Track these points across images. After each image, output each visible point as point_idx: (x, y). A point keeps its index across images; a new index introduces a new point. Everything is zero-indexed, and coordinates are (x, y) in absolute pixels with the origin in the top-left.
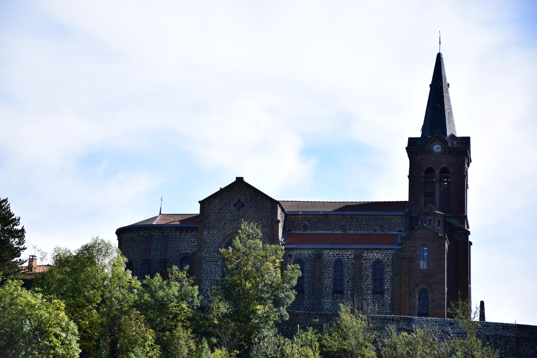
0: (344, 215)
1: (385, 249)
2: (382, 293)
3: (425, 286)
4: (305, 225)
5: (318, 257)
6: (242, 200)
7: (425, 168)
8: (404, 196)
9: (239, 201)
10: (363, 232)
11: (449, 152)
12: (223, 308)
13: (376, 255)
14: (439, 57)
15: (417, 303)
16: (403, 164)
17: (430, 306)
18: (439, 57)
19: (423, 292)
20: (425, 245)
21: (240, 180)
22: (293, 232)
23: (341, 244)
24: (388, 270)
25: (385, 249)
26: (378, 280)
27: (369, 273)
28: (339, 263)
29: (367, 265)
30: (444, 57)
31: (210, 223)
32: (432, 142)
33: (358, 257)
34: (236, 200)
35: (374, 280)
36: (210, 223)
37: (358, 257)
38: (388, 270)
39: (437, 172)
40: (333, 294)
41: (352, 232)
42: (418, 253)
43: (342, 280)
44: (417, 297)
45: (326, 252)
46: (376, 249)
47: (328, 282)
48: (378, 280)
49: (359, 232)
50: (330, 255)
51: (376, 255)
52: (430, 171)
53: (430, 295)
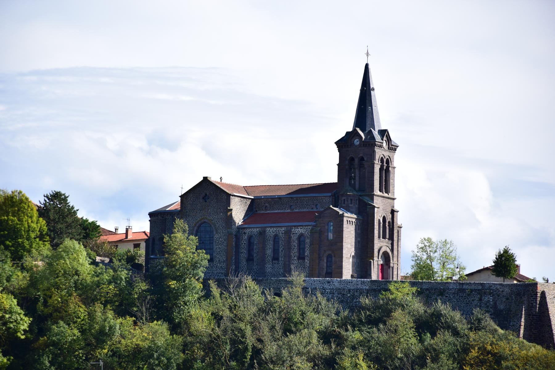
0: (292, 198)
1: (306, 226)
2: (303, 259)
3: (330, 252)
4: (266, 207)
5: (262, 233)
6: (208, 194)
7: (348, 158)
8: (334, 179)
9: (206, 194)
10: (305, 210)
11: (364, 145)
12: (143, 286)
13: (300, 230)
14: (367, 66)
15: (325, 265)
16: (334, 156)
17: (333, 267)
18: (367, 66)
19: (329, 256)
20: (330, 221)
21: (205, 179)
22: (258, 212)
23: (278, 223)
24: (308, 241)
25: (306, 226)
26: (301, 249)
27: (295, 244)
28: (276, 237)
29: (294, 238)
30: (370, 67)
31: (187, 212)
32: (353, 137)
33: (288, 233)
34: (204, 194)
35: (299, 249)
36: (187, 212)
37: (288, 233)
38: (308, 241)
39: (356, 161)
40: (272, 260)
41: (297, 210)
42: (326, 227)
43: (278, 250)
44: (325, 261)
45: (268, 229)
46: (302, 226)
47: (269, 252)
48: (301, 249)
49: (302, 210)
50: (271, 231)
51: (300, 230)
52: (352, 159)
53: (333, 258)
